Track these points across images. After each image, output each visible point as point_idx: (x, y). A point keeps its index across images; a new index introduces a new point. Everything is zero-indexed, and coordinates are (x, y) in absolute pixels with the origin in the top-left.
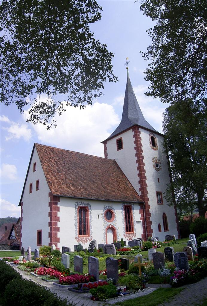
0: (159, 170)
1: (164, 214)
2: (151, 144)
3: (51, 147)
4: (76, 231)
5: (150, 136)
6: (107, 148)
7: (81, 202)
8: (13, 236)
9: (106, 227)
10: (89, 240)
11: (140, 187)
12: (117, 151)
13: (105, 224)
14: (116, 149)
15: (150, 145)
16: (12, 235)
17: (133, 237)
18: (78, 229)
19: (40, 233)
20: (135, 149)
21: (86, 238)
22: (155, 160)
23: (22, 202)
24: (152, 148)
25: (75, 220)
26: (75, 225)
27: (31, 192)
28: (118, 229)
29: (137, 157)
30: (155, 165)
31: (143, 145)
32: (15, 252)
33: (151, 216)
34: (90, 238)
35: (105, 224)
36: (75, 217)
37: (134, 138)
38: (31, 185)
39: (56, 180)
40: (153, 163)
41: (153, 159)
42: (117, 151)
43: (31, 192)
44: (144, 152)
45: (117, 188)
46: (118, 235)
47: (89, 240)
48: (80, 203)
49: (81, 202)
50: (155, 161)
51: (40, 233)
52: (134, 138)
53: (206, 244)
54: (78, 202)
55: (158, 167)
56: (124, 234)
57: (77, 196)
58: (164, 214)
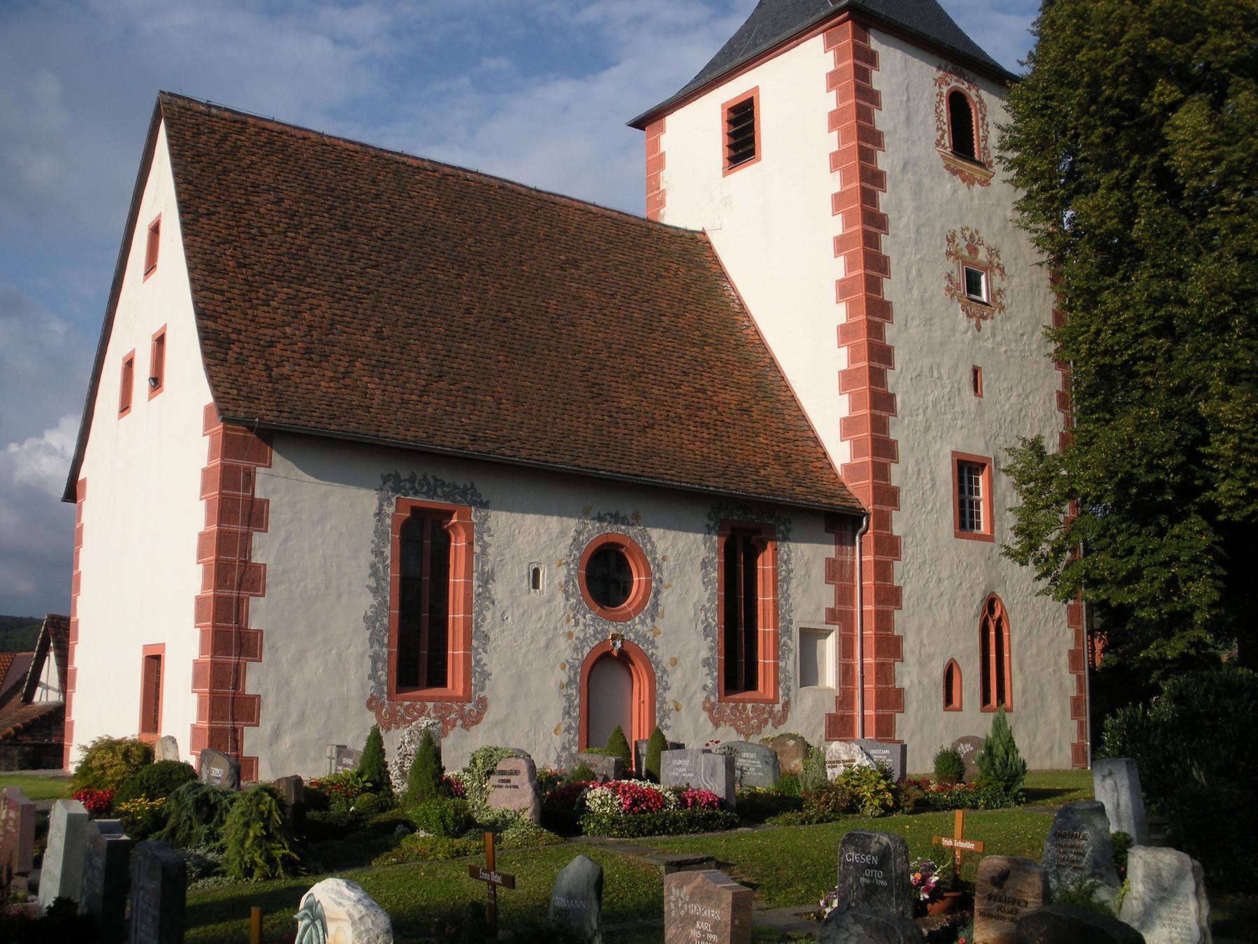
0: (985, 318)
1: (991, 603)
2: (947, 141)
3: (270, 126)
4: (375, 659)
5: (945, 90)
6: (663, 154)
7: (419, 476)
8: (47, 688)
9: (587, 650)
10: (459, 722)
11: (1072, 648)
12: (724, 176)
13: (578, 632)
14: (721, 172)
15: (938, 143)
16: (43, 679)
17: (766, 721)
18: (387, 650)
19: (153, 663)
20: (834, 166)
21: (446, 708)
22: (963, 244)
23: (81, 477)
24: (947, 167)
25: (376, 591)
26: (370, 621)
27: (125, 407)
28: (669, 668)
29: (840, 216)
30: (961, 279)
31: (886, 140)
32: (27, 777)
33: (904, 603)
34: (468, 706)
35: (578, 632)
36: (374, 574)
37: (834, 93)
38: (129, 364)
39: (269, 326)
40: (952, 266)
41: (951, 240)
42: (724, 176)
43: (125, 407)
44: (888, 186)
45: (687, 407)
46: (664, 701)
47: (459, 722)
48: (412, 480)
49: (419, 476)
50: (966, 253)
51: (153, 663)
52: (834, 93)
53: (1255, 513)
54: (397, 476)
55: (978, 293)
56: (708, 698)
57: (393, 433)
58: (991, 603)
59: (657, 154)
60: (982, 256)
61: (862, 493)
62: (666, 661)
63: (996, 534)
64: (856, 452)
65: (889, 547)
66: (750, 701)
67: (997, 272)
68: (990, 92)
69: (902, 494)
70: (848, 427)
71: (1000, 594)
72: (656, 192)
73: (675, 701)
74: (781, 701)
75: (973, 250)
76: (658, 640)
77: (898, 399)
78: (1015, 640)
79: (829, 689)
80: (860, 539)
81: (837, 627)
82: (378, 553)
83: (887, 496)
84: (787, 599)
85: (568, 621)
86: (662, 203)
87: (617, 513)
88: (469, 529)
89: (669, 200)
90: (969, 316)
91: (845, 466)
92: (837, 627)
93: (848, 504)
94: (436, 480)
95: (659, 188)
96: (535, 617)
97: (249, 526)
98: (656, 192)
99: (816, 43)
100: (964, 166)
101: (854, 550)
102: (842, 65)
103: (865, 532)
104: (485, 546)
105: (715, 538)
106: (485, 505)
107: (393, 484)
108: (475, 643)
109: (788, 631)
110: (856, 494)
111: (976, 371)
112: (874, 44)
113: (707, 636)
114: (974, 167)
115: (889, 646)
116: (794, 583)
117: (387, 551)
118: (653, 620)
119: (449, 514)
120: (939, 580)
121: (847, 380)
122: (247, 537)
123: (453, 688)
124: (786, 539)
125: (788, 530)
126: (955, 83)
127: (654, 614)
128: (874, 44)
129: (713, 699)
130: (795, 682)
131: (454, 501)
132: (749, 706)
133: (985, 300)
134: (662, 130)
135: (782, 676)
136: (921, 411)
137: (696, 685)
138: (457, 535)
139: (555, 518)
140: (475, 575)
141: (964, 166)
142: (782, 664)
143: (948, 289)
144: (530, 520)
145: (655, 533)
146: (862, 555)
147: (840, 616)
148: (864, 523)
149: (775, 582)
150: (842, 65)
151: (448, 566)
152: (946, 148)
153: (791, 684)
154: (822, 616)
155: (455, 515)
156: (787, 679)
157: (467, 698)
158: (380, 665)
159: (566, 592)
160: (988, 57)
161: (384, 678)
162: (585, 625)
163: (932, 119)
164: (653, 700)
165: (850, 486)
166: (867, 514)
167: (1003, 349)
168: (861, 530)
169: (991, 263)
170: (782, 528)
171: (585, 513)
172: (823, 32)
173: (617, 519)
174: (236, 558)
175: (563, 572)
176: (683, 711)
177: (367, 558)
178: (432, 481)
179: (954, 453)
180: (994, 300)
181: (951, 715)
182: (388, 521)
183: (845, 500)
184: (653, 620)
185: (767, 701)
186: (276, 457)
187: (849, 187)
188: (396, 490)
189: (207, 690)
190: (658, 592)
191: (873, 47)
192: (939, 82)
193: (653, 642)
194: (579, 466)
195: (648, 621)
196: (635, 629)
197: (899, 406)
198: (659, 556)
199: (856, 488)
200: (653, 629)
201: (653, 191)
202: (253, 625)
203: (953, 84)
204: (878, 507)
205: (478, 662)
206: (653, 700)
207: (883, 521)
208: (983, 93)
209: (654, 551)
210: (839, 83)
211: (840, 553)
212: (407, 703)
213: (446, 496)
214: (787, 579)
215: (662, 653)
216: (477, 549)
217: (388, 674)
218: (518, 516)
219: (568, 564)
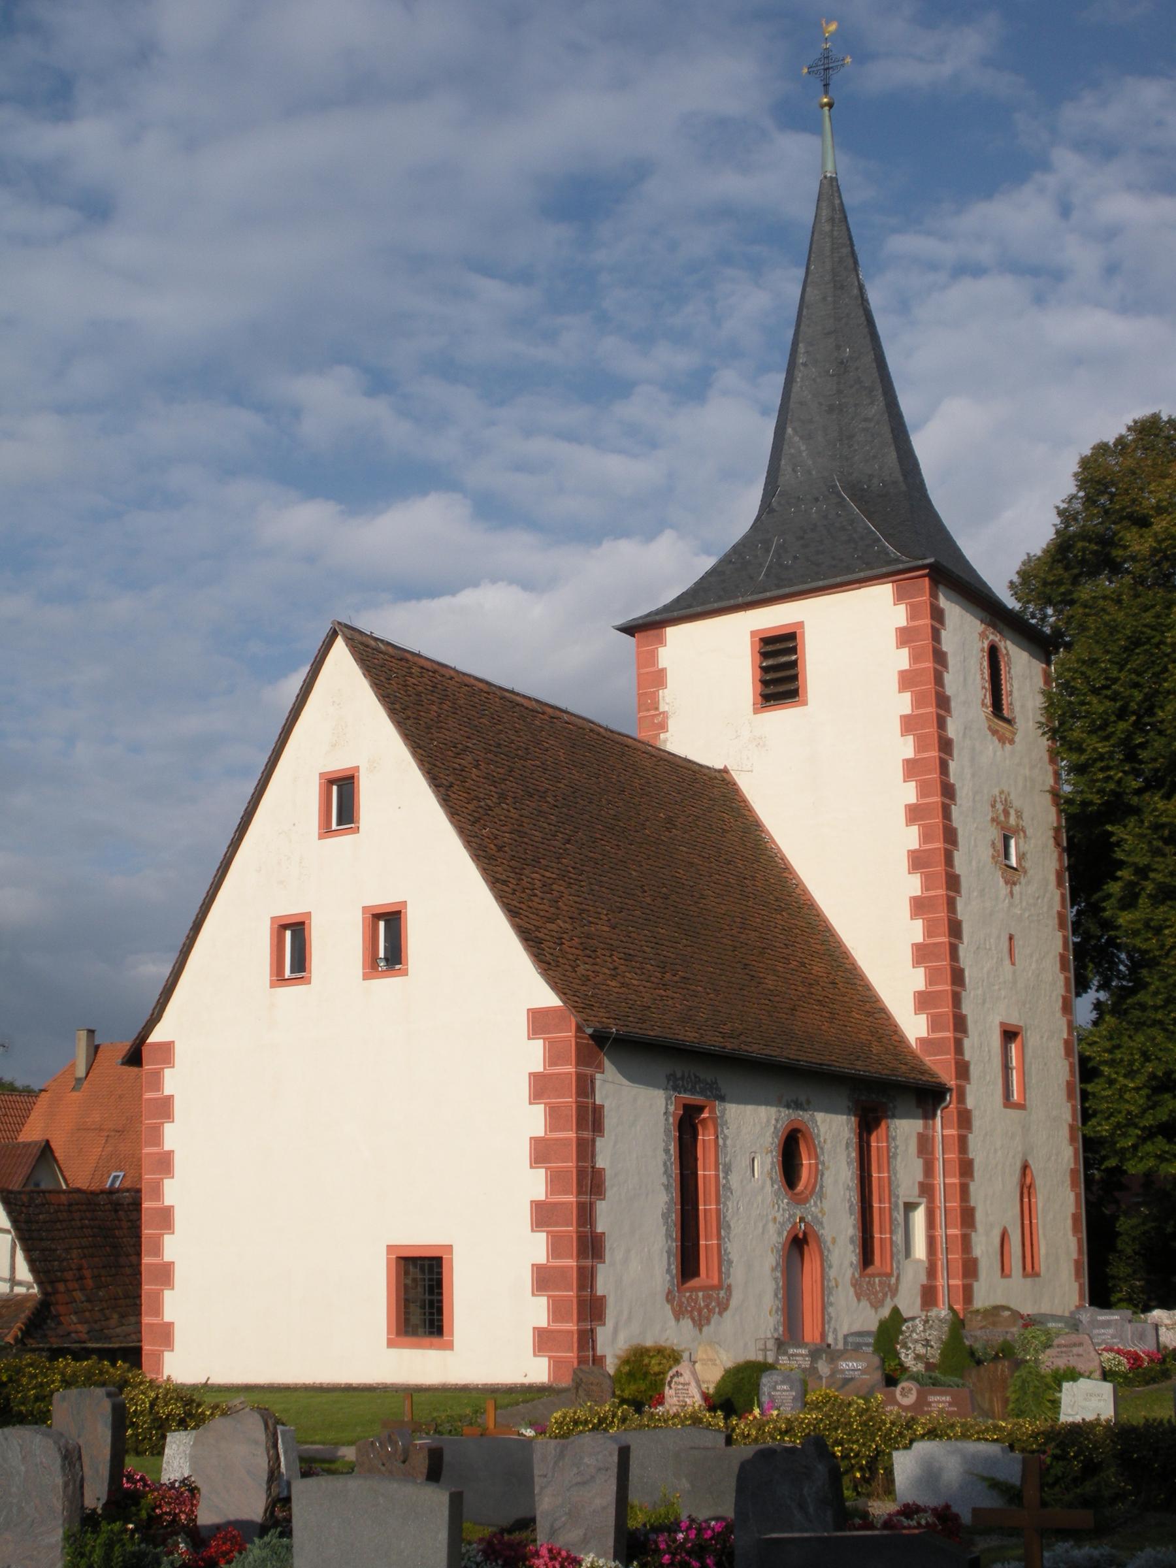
9: (785, 1233)
14: (751, 708)
57: (688, 1036)
58: (1025, 1167)
59: (654, 669)
60: (1012, 820)
61: (941, 1068)
62: (829, 1239)
63: (1027, 1103)
64: (934, 1025)
65: (965, 1119)
66: (701, 1289)
67: (1022, 834)
68: (1013, 643)
69: (972, 1068)
70: (923, 1001)
71: (1030, 1162)
72: (653, 712)
73: (835, 1279)
74: (895, 1274)
75: (1006, 813)
76: (825, 1220)
77: (967, 973)
78: (1040, 1205)
79: (920, 1261)
80: (942, 1112)
81: (925, 1200)
82: (667, 1151)
83: (963, 1070)
84: (895, 1176)
85: (774, 1206)
86: (663, 727)
87: (797, 1099)
88: (714, 1120)
89: (672, 724)
90: (1007, 883)
91: (921, 1040)
92: (925, 1200)
93: (934, 1080)
94: (696, 1077)
95: (657, 709)
96: (755, 1205)
97: (594, 1132)
98: (653, 712)
99: (883, 592)
100: (999, 726)
101: (934, 1125)
102: (916, 623)
103: (946, 1107)
104: (725, 1138)
105: (853, 1118)
106: (722, 1099)
107: (674, 1084)
108: (723, 1233)
109: (897, 1205)
110: (936, 1069)
111: (1011, 938)
112: (943, 602)
113: (851, 1214)
114: (1001, 723)
115: (968, 1217)
116: (899, 1158)
117: (672, 1148)
118: (821, 1202)
119: (701, 1109)
120: (996, 1151)
121: (921, 954)
122: (594, 1141)
123: (707, 1276)
124: (893, 1116)
125: (895, 1107)
126: (996, 638)
127: (821, 1197)
128: (943, 602)
129: (857, 1275)
130: (902, 1256)
131: (706, 1097)
132: (700, 1294)
133: (1015, 866)
134: (661, 641)
135: (895, 1250)
136: (980, 984)
137: (846, 1263)
138: (704, 1129)
139: (763, 1107)
140: (721, 1167)
141: (999, 726)
142: (894, 1238)
143: (993, 857)
144: (749, 1108)
145: (820, 1116)
146: (941, 1128)
147: (926, 1189)
148: (948, 1098)
149: (889, 1157)
150: (916, 623)
151: (696, 1159)
152: (987, 708)
153: (900, 1257)
154: (916, 1191)
155: (707, 1110)
156: (898, 1252)
157: (719, 1287)
158: (672, 1259)
159: (771, 1179)
160: (993, 593)
161: (674, 1271)
162: (783, 1210)
163: (979, 677)
164: (823, 1277)
165: (928, 1060)
166: (950, 1090)
167: (1027, 915)
168: (943, 1105)
169: (1018, 825)
170: (891, 1105)
171: (779, 1102)
172: (893, 582)
173: (797, 1105)
174: (588, 1164)
175: (769, 1159)
176: (840, 1288)
177: (662, 1156)
178: (693, 1077)
179: (1002, 1024)
180: (1021, 865)
181: (1005, 1280)
182: (671, 1120)
183: (923, 1073)
184: (821, 1202)
185: (712, 1288)
186: (607, 1063)
187: (925, 755)
188: (675, 1089)
189: (572, 1293)
190: (822, 1175)
191: (942, 605)
192: (983, 635)
193: (821, 1223)
194: (788, 1058)
195: (819, 1203)
196: (812, 1208)
197: (967, 980)
198: (822, 1139)
199: (935, 1062)
200: (822, 1211)
201: (648, 710)
202: (599, 1230)
203: (991, 637)
204: (959, 1082)
205: (725, 1251)
206: (823, 1277)
207: (962, 1098)
208: (1008, 643)
209: (818, 1135)
210: (913, 641)
211: (926, 1127)
212: (688, 1294)
213: (702, 1093)
214: (895, 1155)
215: (826, 1233)
216: (721, 1142)
217: (677, 1267)
218: (742, 1107)
219: (771, 1151)
